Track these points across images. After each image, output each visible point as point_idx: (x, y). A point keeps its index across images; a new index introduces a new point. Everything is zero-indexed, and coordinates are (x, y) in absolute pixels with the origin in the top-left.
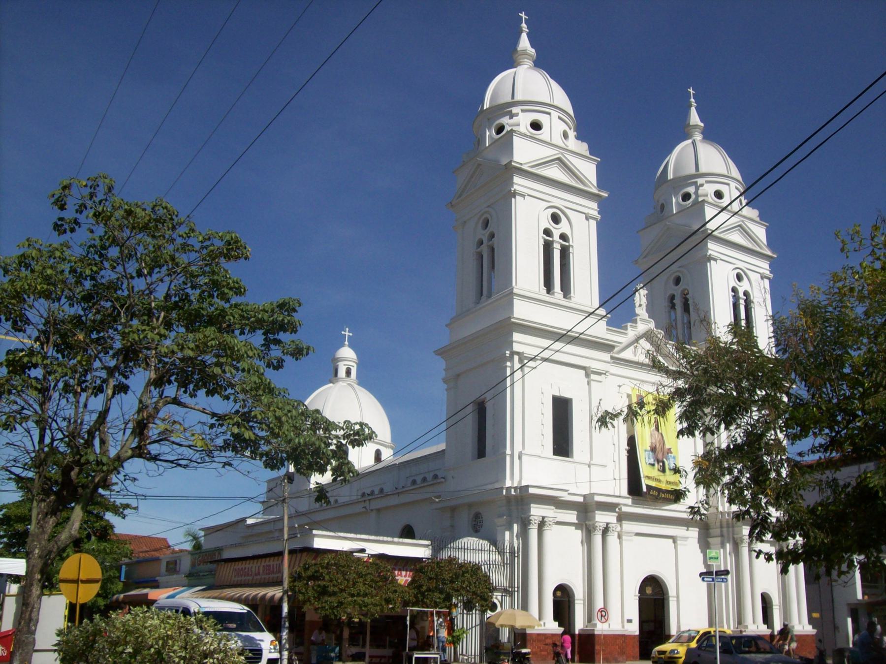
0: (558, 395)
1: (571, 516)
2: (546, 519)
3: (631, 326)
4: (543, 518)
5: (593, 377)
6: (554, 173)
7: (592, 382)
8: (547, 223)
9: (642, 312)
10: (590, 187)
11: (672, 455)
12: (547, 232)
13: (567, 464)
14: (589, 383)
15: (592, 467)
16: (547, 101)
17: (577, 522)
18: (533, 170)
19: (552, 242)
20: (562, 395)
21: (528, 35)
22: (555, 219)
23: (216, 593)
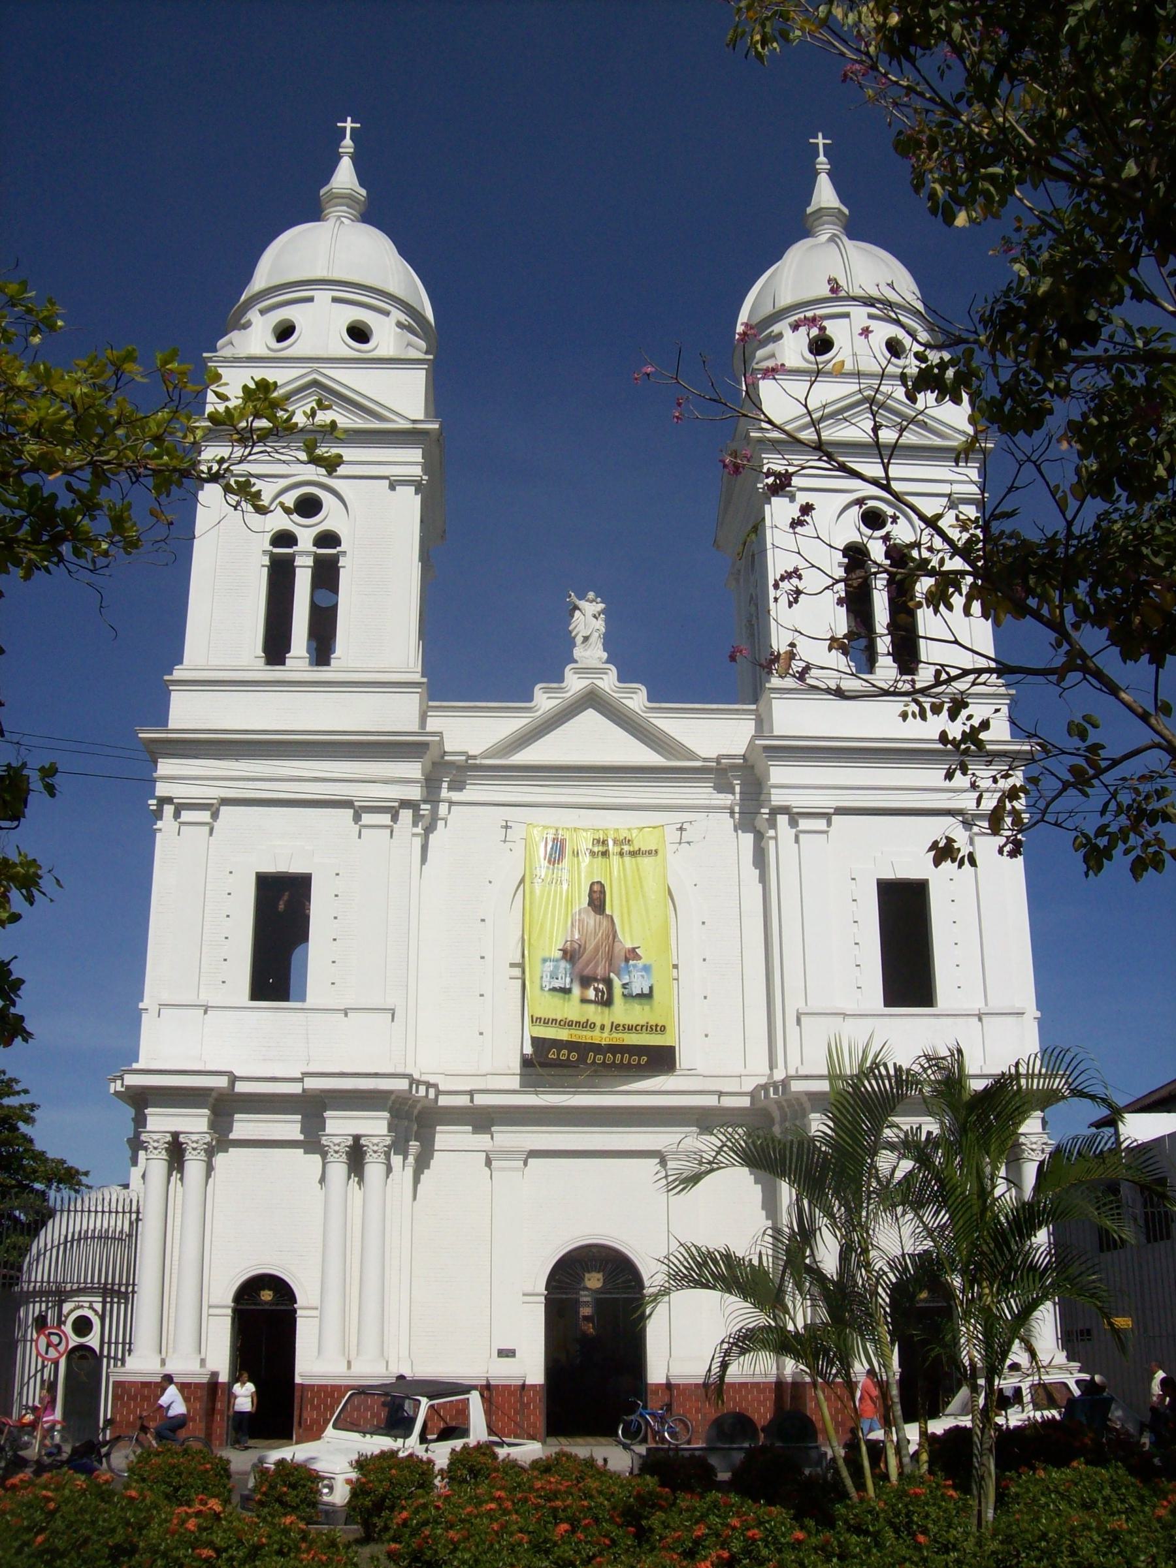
1: (289, 1127)
3: (546, 690)
4: (357, 1138)
5: (804, 824)
9: (591, 653)
10: (394, 421)
11: (640, 963)
15: (985, 1019)
17: (301, 1137)
19: (290, 560)
20: (899, 876)
21: (830, 174)
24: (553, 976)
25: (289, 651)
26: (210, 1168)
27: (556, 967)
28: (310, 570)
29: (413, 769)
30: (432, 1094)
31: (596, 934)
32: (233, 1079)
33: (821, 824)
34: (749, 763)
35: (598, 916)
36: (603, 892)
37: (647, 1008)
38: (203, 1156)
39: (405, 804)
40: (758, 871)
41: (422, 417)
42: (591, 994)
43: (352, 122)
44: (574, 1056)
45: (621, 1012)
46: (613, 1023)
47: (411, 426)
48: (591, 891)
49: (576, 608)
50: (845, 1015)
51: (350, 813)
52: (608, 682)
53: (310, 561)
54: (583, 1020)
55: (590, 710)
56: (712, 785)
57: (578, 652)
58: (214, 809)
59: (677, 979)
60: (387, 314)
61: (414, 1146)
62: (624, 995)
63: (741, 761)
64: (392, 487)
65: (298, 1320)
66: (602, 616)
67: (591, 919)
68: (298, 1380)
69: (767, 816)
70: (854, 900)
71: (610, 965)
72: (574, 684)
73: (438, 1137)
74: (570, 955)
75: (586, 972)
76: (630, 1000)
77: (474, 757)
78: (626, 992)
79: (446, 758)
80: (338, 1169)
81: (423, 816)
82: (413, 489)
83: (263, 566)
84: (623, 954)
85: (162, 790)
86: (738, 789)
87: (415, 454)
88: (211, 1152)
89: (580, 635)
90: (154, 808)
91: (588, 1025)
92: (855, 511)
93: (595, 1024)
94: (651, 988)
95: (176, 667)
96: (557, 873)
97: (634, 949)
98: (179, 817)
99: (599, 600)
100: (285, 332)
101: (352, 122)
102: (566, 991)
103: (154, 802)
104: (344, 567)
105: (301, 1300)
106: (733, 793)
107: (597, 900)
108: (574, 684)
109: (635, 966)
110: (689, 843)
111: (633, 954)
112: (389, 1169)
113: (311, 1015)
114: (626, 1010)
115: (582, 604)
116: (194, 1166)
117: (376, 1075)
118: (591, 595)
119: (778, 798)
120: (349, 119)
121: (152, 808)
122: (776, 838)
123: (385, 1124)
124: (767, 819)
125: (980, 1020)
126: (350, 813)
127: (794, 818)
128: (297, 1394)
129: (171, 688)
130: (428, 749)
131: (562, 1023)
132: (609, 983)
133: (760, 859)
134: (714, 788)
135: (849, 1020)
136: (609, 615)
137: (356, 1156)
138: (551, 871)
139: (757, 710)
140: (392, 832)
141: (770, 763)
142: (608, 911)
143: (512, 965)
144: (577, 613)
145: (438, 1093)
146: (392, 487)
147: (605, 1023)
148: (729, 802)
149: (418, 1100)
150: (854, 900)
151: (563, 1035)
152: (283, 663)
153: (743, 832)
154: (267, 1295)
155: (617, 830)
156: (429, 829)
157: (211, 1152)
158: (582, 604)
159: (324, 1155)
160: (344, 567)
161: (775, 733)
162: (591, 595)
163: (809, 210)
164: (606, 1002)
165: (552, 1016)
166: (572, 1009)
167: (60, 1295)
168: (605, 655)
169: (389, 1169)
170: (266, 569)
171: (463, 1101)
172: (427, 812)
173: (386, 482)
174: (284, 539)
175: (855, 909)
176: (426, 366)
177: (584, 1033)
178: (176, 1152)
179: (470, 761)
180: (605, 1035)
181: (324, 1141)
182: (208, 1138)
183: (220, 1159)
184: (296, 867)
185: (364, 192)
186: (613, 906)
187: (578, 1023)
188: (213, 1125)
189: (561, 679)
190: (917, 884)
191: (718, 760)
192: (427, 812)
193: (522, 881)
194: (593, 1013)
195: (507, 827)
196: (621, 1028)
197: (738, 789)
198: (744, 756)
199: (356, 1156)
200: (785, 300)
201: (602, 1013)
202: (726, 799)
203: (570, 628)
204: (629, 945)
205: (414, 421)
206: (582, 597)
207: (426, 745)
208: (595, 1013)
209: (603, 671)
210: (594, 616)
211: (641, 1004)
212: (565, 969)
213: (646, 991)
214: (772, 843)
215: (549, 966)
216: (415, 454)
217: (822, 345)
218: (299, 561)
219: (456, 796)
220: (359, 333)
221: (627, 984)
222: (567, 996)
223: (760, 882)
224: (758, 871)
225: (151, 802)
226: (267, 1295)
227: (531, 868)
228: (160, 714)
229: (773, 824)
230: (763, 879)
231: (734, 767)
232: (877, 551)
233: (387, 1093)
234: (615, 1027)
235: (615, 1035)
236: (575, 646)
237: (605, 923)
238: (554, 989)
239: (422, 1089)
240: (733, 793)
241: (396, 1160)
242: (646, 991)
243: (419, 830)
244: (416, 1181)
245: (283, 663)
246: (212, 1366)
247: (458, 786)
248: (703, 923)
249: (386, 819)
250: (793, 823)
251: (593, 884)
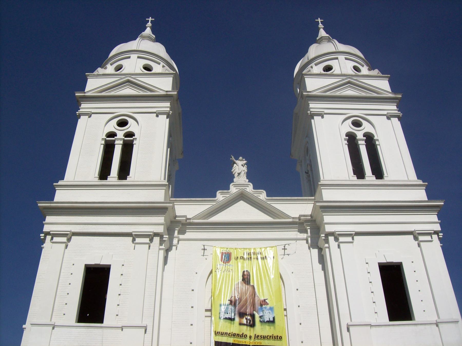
0: (385, 262)
3: (222, 193)
5: (341, 239)
6: (128, 91)
7: (421, 243)
8: (112, 127)
11: (268, 307)
14: (419, 245)
15: (440, 325)
20: (388, 261)
24: (226, 312)
25: (110, 175)
27: (227, 308)
28: (121, 145)
29: (160, 219)
31: (246, 294)
33: (349, 239)
34: (313, 219)
35: (247, 286)
36: (249, 275)
37: (272, 327)
39: (156, 234)
40: (321, 265)
41: (171, 90)
42: (244, 321)
43: (151, 18)
45: (259, 329)
46: (255, 335)
47: (166, 93)
48: (243, 275)
49: (235, 163)
50: (371, 326)
52: (250, 189)
53: (121, 142)
54: (241, 333)
55: (242, 201)
56: (297, 230)
57: (235, 180)
58: (69, 236)
59: (286, 316)
60: (159, 64)
62: (261, 321)
63: (310, 218)
64: (157, 116)
66: (245, 165)
67: (245, 287)
69: (324, 238)
70: (376, 313)
71: (254, 307)
72: (233, 190)
74: (233, 303)
75: (242, 310)
76: (264, 324)
77: (190, 219)
78: (262, 320)
79: (177, 219)
81: (165, 241)
82: (166, 116)
83: (102, 144)
84: (259, 302)
85: (46, 228)
86: (309, 231)
89: (237, 173)
90: (43, 237)
91: (243, 336)
92: (350, 121)
93: (247, 336)
94: (274, 318)
95: (60, 181)
96: (227, 267)
97: (265, 300)
98: (52, 240)
99: (244, 159)
100: (119, 68)
101: (151, 18)
102: (232, 320)
103: (43, 235)
104: (135, 144)
106: (307, 233)
107: (246, 279)
109: (265, 308)
110: (288, 255)
111: (264, 303)
114: (262, 328)
118: (241, 158)
119: (329, 228)
120: (150, 18)
121: (42, 237)
122: (329, 248)
124: (324, 239)
125: (437, 326)
127: (336, 237)
129: (56, 188)
130: (167, 210)
131: (230, 335)
132: (253, 316)
133: (322, 260)
134: (298, 231)
135: (374, 329)
138: (224, 266)
139: (315, 199)
140: (149, 246)
141: (323, 214)
142: (252, 284)
143: (207, 310)
146: (157, 116)
147: (252, 335)
148: (305, 237)
150: (376, 313)
152: (107, 179)
153: (313, 249)
155: (255, 249)
156: (168, 251)
160: (135, 144)
161: (324, 200)
165: (225, 331)
166: (235, 328)
170: (103, 145)
172: (166, 239)
173: (155, 114)
174: (112, 135)
175: (373, 296)
176: (173, 76)
177: (241, 340)
179: (187, 221)
180: (252, 341)
184: (104, 262)
185: (154, 36)
186: (254, 281)
187: (238, 335)
189: (228, 189)
190: (397, 266)
191: (299, 218)
192: (166, 239)
193: (211, 272)
194: (245, 330)
195: (204, 249)
196: (260, 337)
197: (309, 231)
198: (311, 215)
201: (250, 330)
202: (304, 236)
203: (232, 171)
204: (262, 298)
205: (167, 91)
206: (237, 159)
208: (247, 330)
209: (247, 186)
210: (242, 165)
211: (269, 326)
212: (231, 309)
213: (272, 319)
214: (327, 250)
215: (223, 308)
217: (328, 68)
218: (116, 142)
219: (181, 237)
220: (147, 68)
221: (262, 316)
222: (232, 322)
223: (322, 270)
224: (321, 265)
225: (41, 235)
227: (215, 265)
228: (51, 196)
229: (327, 241)
230: (324, 268)
231: (307, 221)
232: (360, 135)
234: (257, 337)
235: (257, 341)
236: (234, 177)
237: (250, 289)
238: (226, 318)
240: (307, 233)
242: (272, 319)
245: (107, 179)
247: (182, 232)
248: (297, 290)
249: (147, 240)
250: (336, 239)
251: (244, 272)
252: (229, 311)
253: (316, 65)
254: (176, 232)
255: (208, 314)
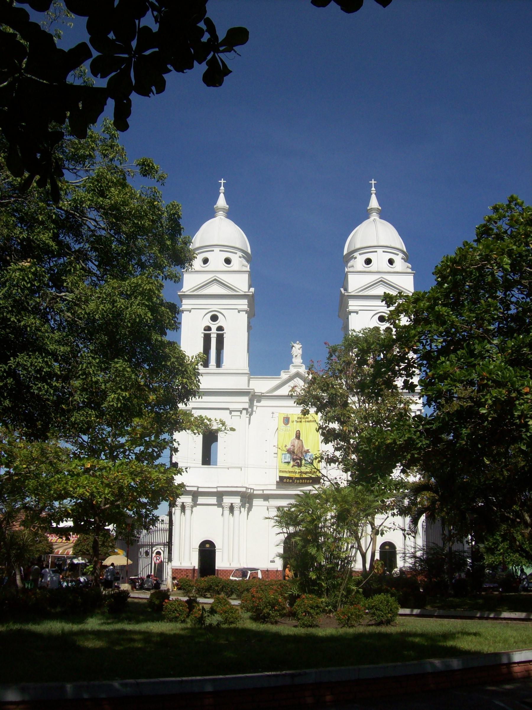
1: (213, 500)
2: (185, 504)
3: (284, 372)
4: (232, 504)
8: (207, 322)
9: (298, 360)
12: (208, 328)
13: (210, 469)
16: (375, 244)
18: (360, 294)
19: (210, 334)
22: (214, 318)
23: (452, 612)
26: (192, 511)
29: (246, 399)
30: (252, 491)
32: (198, 487)
38: (190, 509)
39: (244, 409)
44: (291, 481)
47: (244, 293)
49: (293, 346)
51: (229, 411)
57: (294, 360)
61: (247, 505)
64: (239, 312)
65: (217, 553)
68: (216, 568)
72: (293, 370)
73: (254, 502)
80: (227, 512)
87: (245, 302)
88: (192, 507)
105: (217, 547)
107: (298, 436)
108: (293, 370)
112: (240, 512)
113: (219, 469)
115: (295, 345)
116: (188, 511)
117: (237, 487)
123: (239, 500)
126: (229, 411)
128: (216, 572)
136: (304, 349)
137: (232, 508)
142: (301, 439)
143: (275, 453)
144: (294, 348)
145: (254, 490)
146: (239, 312)
149: (248, 493)
151: (287, 475)
154: (208, 546)
156: (250, 415)
157: (192, 507)
158: (295, 345)
159: (223, 508)
162: (298, 342)
163: (368, 208)
164: (300, 465)
167: (152, 546)
168: (302, 361)
169: (240, 512)
171: (261, 492)
174: (208, 328)
178: (183, 508)
181: (223, 505)
182: (192, 504)
183: (194, 509)
185: (228, 206)
188: (193, 500)
189: (288, 369)
193: (277, 429)
194: (297, 469)
199: (232, 508)
200: (358, 246)
206: (295, 342)
207: (250, 392)
209: (301, 366)
216: (245, 302)
219: (258, 404)
226: (208, 546)
233: (240, 492)
237: (300, 442)
238: (285, 462)
239: (249, 490)
241: (242, 509)
243: (248, 416)
244: (248, 514)
246: (193, 565)
247: (259, 401)
249: (239, 413)
252: (287, 457)
253: (360, 254)
254: (255, 401)
255: (276, 455)
